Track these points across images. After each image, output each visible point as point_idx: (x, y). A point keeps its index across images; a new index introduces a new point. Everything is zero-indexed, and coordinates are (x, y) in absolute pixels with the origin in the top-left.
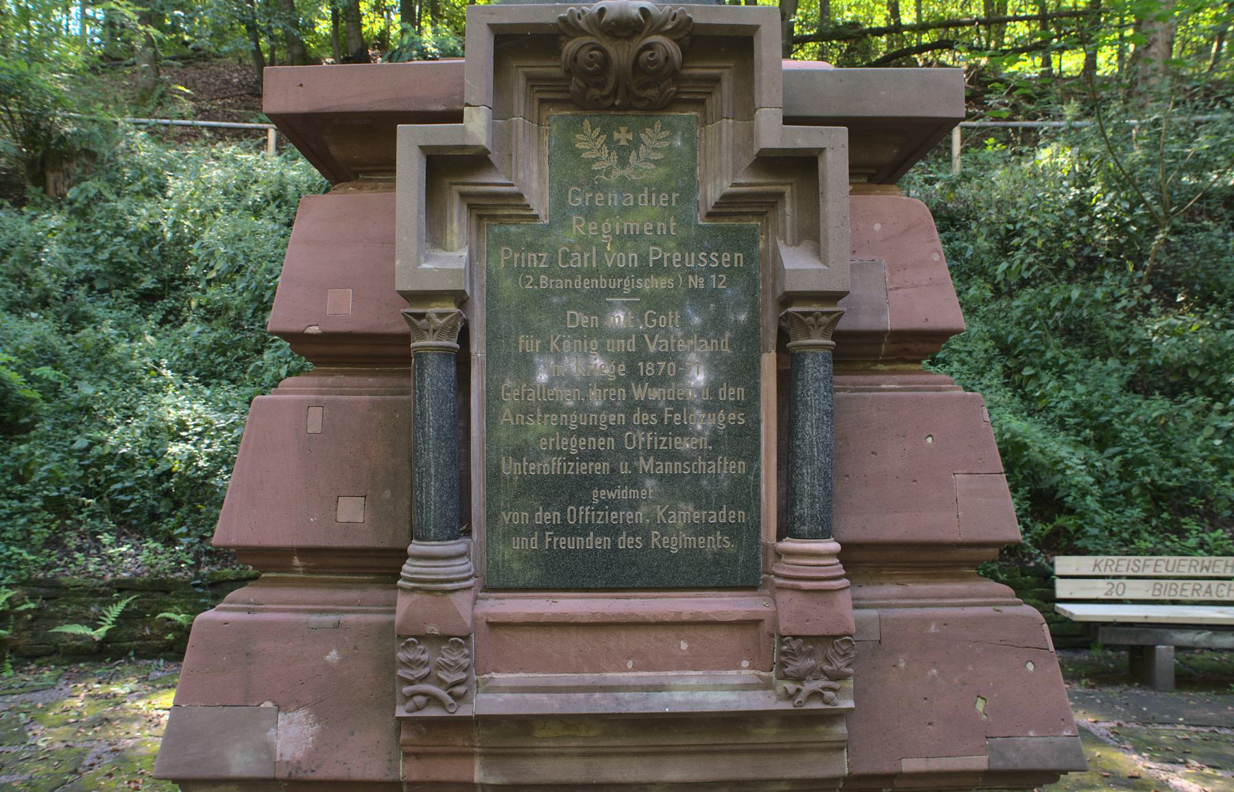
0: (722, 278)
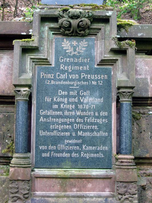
0: (101, 82)
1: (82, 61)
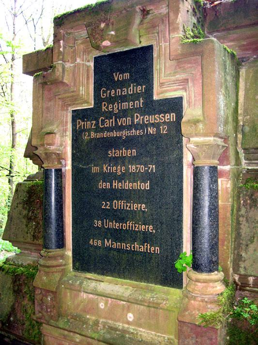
1: (133, 91)
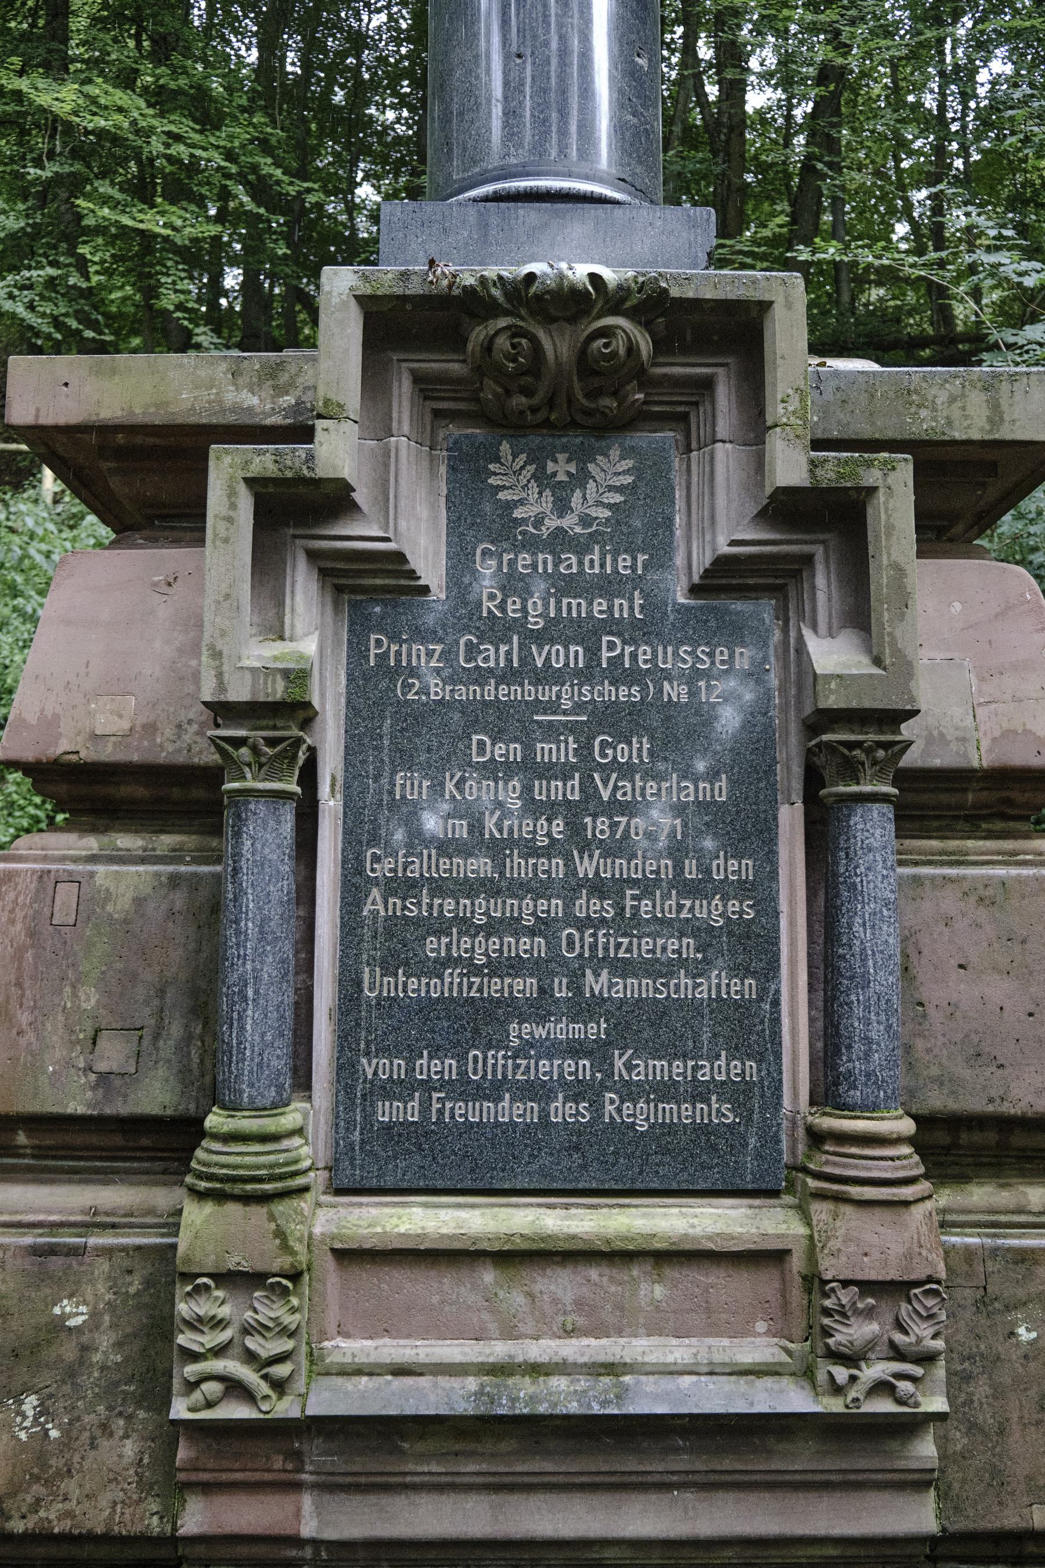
1: (602, 566)
